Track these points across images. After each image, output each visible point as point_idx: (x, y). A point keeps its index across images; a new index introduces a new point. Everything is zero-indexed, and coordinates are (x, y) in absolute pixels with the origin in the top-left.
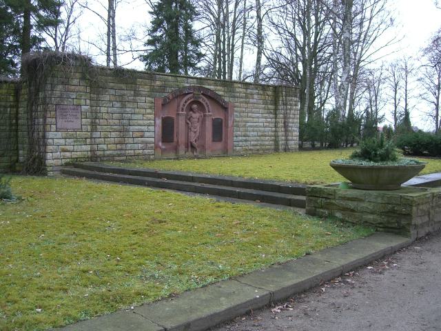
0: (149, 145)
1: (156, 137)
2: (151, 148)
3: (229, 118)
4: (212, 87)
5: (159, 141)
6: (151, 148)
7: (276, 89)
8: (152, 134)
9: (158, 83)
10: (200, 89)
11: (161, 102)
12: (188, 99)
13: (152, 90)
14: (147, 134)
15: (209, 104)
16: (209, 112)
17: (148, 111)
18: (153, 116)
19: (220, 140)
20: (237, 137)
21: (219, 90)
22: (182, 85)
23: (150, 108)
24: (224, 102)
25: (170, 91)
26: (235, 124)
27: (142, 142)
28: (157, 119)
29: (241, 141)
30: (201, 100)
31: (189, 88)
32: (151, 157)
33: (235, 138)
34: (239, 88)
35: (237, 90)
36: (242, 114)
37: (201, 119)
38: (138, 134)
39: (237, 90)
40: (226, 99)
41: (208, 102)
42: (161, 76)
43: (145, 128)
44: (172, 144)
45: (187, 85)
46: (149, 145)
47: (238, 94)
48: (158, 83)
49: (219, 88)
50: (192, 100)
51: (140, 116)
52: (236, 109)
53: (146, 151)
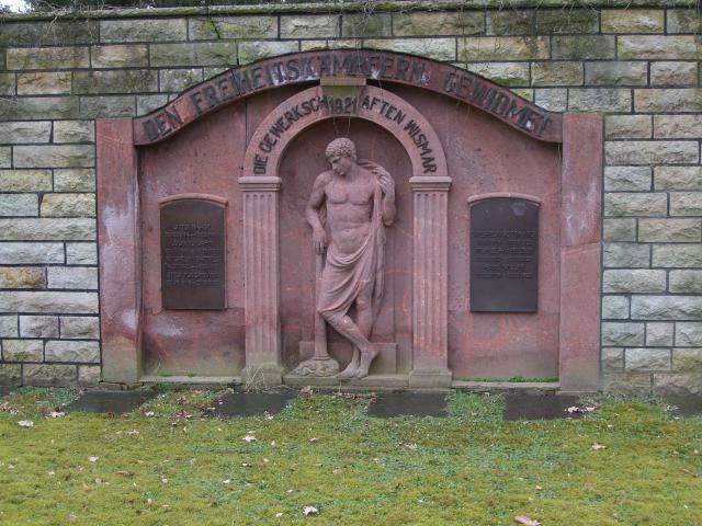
0: (69, 324)
1: (107, 288)
2: (85, 335)
3: (370, 260)
4: (440, 47)
5: (122, 307)
6: (85, 335)
7: (605, 139)
8: (86, 277)
9: (112, 55)
10: (357, 61)
11: (123, 142)
12: (293, 116)
13: (86, 87)
14: (57, 277)
15: (423, 123)
16: (429, 167)
17: (65, 178)
18: (91, 198)
19: (527, 306)
20: (627, 294)
21: (495, 58)
22: (245, 51)
23: (75, 165)
24: (529, 111)
25: (179, 84)
26: (612, 227)
27: (37, 312)
28: (107, 210)
29: (662, 317)
30: (374, 115)
31: (291, 60)
32: (84, 370)
33: (614, 304)
34: (646, 31)
35: (628, 44)
36: (663, 174)
37: (382, 209)
38: (19, 275)
39: (628, 44)
40: (546, 101)
41: (423, 123)
42: (126, 24)
43: (53, 252)
44: (215, 317)
45: (277, 48)
46: (69, 324)
47: (638, 69)
48: (112, 55)
49: (488, 44)
50: (319, 116)
51: (27, 202)
52: (613, 148)
53: (58, 349)
